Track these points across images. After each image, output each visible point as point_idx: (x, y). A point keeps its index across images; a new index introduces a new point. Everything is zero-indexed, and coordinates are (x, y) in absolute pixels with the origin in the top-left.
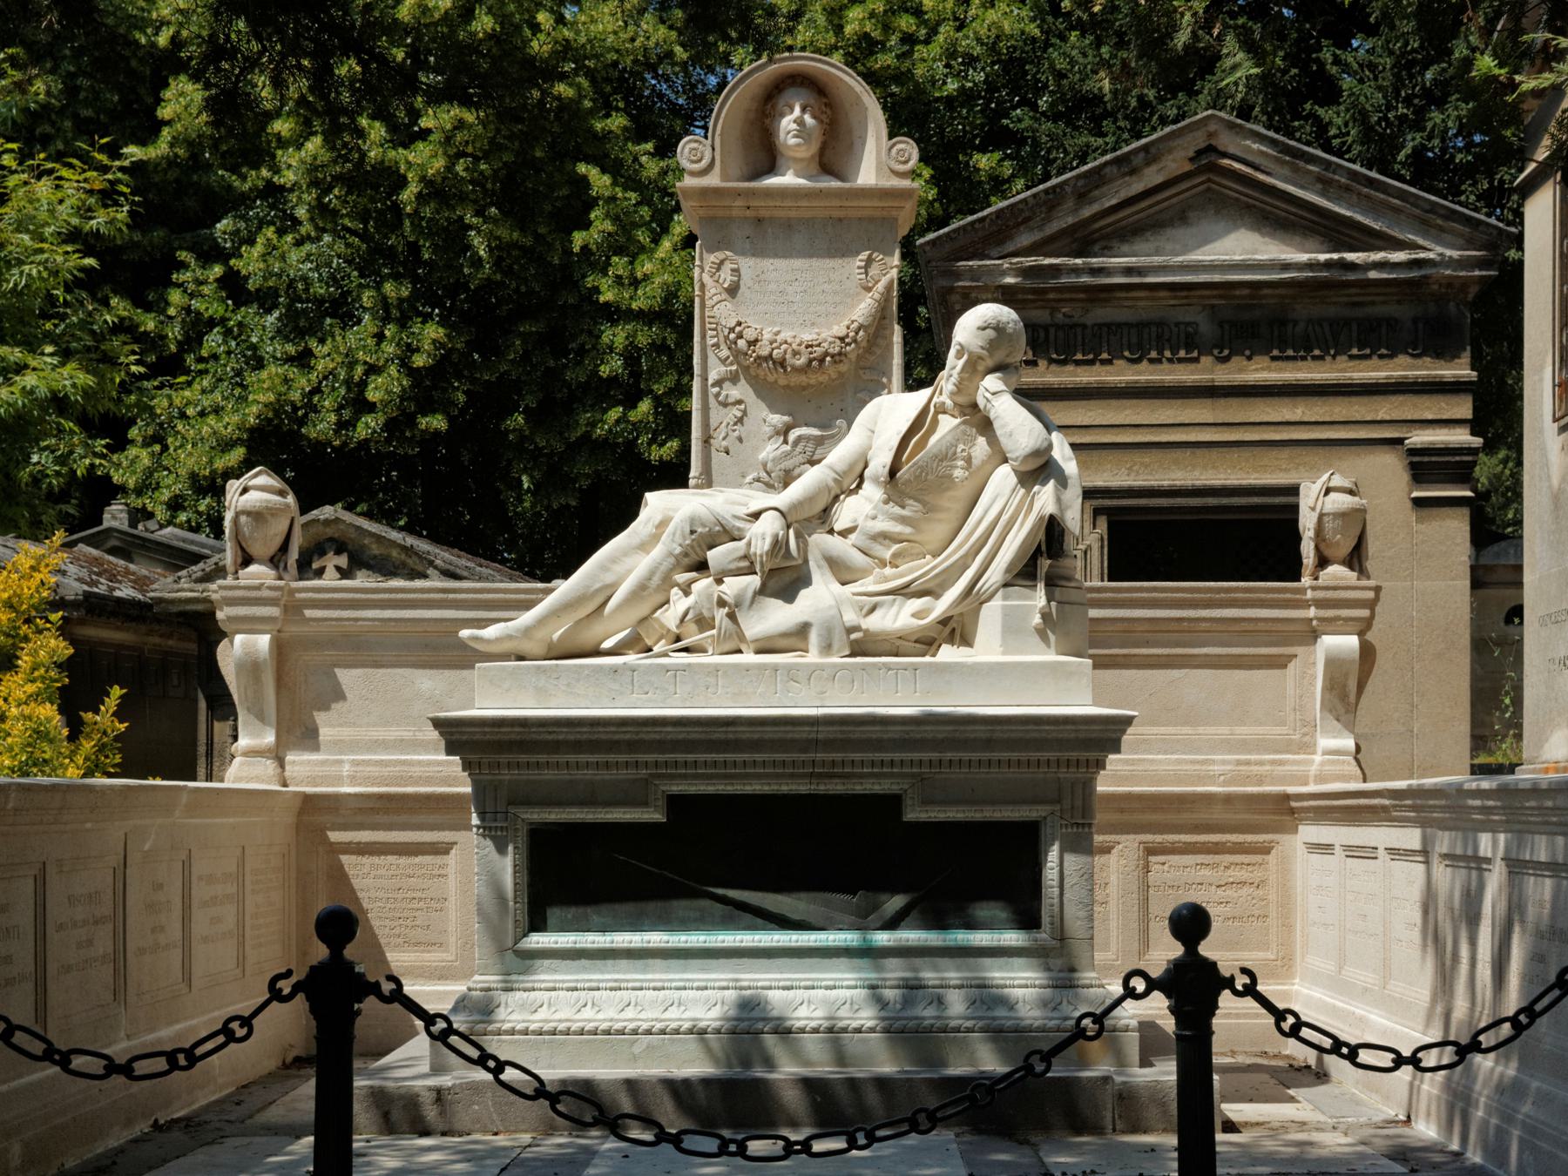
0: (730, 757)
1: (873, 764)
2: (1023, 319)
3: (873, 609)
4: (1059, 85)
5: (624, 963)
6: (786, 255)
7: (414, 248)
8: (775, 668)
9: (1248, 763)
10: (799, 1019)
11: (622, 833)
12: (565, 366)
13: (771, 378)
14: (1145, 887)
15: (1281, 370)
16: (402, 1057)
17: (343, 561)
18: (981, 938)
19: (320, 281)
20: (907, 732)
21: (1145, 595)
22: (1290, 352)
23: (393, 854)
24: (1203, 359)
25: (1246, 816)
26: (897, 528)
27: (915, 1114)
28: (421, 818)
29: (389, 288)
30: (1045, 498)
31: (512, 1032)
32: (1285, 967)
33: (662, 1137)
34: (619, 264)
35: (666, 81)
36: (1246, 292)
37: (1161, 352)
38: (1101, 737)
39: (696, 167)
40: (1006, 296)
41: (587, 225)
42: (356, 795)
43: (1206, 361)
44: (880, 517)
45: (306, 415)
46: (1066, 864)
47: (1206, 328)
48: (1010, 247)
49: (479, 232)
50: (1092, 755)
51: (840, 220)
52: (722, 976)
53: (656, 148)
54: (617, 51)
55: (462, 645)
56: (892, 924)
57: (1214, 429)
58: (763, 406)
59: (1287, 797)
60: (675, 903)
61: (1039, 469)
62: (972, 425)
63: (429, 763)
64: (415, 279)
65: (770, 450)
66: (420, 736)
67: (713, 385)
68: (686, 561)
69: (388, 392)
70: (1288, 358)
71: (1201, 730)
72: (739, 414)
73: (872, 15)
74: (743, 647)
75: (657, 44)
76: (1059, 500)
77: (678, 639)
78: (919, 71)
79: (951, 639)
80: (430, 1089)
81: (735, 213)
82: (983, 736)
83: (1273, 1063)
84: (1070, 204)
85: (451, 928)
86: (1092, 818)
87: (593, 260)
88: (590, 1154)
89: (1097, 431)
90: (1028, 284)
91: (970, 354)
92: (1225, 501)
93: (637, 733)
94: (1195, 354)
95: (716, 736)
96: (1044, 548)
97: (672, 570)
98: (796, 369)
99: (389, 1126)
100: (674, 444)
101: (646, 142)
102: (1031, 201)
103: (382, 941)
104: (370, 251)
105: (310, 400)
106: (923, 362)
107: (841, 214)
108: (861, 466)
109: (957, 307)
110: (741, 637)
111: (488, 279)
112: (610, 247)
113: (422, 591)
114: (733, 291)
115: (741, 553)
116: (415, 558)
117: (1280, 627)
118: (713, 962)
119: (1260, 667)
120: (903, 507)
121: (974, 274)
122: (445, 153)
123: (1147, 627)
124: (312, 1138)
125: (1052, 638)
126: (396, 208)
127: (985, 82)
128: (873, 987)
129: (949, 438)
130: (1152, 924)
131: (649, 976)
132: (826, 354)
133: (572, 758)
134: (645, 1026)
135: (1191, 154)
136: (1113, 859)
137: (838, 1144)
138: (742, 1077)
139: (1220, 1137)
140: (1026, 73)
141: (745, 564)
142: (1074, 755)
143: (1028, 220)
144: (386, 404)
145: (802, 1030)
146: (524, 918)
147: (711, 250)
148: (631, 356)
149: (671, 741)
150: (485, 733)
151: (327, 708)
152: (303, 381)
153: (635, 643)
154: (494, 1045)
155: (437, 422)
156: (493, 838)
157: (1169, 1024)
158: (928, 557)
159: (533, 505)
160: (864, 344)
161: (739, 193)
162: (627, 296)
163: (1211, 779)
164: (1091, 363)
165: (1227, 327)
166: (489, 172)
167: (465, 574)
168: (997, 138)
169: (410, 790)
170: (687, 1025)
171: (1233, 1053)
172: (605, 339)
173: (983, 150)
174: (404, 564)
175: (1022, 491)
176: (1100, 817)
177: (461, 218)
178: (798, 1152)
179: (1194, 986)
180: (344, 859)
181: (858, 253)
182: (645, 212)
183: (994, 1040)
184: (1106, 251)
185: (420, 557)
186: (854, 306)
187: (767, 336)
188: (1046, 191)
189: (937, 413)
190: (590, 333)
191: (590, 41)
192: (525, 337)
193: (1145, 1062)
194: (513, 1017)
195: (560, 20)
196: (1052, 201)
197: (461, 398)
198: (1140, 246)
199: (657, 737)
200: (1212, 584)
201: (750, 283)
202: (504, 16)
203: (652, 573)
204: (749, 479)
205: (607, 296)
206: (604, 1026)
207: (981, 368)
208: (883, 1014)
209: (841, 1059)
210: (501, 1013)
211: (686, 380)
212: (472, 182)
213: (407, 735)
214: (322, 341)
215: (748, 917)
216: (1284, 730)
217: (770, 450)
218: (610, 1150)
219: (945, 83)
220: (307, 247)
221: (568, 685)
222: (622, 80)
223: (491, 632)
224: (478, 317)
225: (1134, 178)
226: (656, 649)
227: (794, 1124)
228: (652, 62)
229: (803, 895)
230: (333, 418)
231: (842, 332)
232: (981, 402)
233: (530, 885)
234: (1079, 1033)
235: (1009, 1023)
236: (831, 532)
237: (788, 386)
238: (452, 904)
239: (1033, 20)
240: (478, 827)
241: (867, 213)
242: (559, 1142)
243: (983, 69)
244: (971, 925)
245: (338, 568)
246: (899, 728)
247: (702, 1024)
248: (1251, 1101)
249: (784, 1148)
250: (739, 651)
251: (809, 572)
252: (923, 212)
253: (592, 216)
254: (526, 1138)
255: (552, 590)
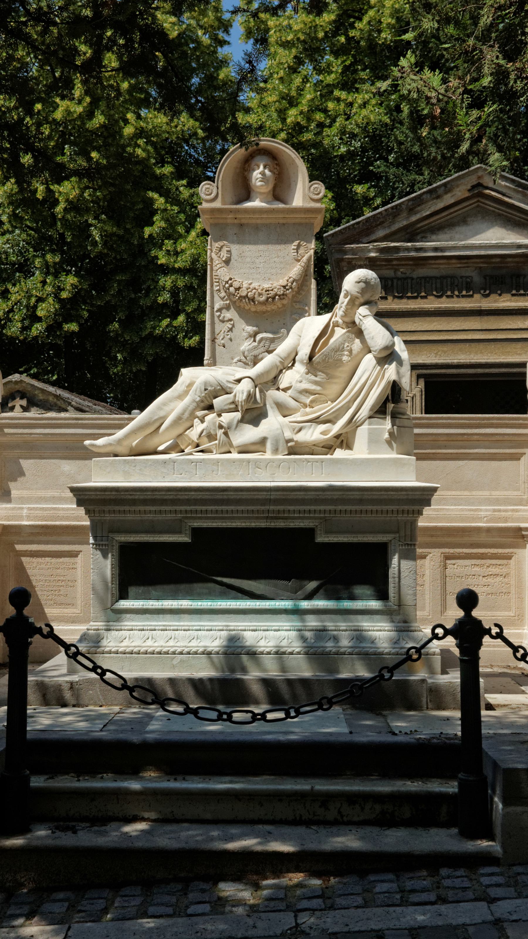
0: (224, 508)
1: (300, 512)
2: (378, 275)
3: (300, 430)
4: (400, 149)
5: (168, 616)
6: (255, 243)
7: (62, 236)
8: (249, 461)
9: (499, 511)
10: (260, 647)
11: (173, 548)
12: (140, 297)
13: (247, 308)
14: (444, 577)
15: (517, 301)
16: (52, 664)
17: (24, 402)
18: (359, 605)
19: (13, 254)
20: (318, 495)
21: (444, 421)
22: (522, 292)
23: (48, 556)
24: (475, 295)
25: (499, 539)
26: (313, 387)
27: (321, 699)
28: (64, 538)
29: (49, 257)
30: (391, 371)
31: (110, 652)
32: (519, 620)
33: (188, 710)
34: (168, 244)
35: (193, 148)
36: (498, 260)
37: (453, 292)
38: (421, 498)
39: (208, 197)
40: (371, 264)
41: (152, 224)
42: (30, 526)
43: (477, 296)
44: (304, 381)
45: (5, 323)
46: (402, 565)
47: (477, 279)
48: (373, 237)
49: (96, 228)
50: (416, 508)
51: (284, 224)
52: (220, 624)
53: (188, 183)
54: (168, 133)
55: (85, 448)
56: (310, 597)
57: (481, 332)
58: (243, 321)
59: (520, 529)
60: (196, 585)
61: (388, 356)
62: (353, 333)
63: (68, 509)
64: (62, 252)
65: (246, 345)
66: (63, 495)
67: (217, 311)
68: (202, 405)
69: (48, 311)
70: (521, 295)
71: (474, 493)
72: (230, 326)
73: (301, 113)
74: (232, 450)
75: (189, 129)
76: (398, 373)
77: (198, 446)
78: (326, 142)
79: (341, 446)
80: (67, 682)
81: (229, 221)
82: (358, 497)
83: (513, 672)
84: (404, 214)
85: (78, 596)
86: (415, 540)
87: (155, 242)
88: (150, 717)
89: (418, 334)
90: (383, 256)
91: (352, 295)
92: (487, 371)
93: (176, 495)
94: (471, 293)
95: (218, 497)
96: (390, 398)
97: (194, 410)
98: (260, 303)
99: (46, 701)
100: (197, 338)
101: (183, 180)
102: (384, 213)
103: (43, 602)
104: (40, 238)
105: (8, 316)
106: (328, 295)
107: (284, 221)
108: (294, 354)
109: (345, 269)
110: (231, 445)
111: (101, 252)
112: (163, 235)
113: (65, 419)
114: (227, 262)
115: (231, 401)
116: (61, 401)
117: (516, 438)
118: (215, 616)
119: (505, 460)
120: (316, 376)
121: (353, 251)
122: (79, 187)
123: (445, 438)
124: (6, 708)
125: (395, 445)
126: (54, 216)
127: (361, 147)
128: (299, 630)
129: (340, 340)
130: (448, 596)
131: (182, 624)
132: (276, 295)
133: (142, 508)
134: (179, 650)
135: (469, 187)
136: (427, 562)
137: (281, 715)
138: (230, 677)
139: (484, 713)
140: (382, 142)
141: (233, 406)
142: (406, 508)
143: (383, 222)
144: (47, 317)
145: (262, 653)
146: (116, 592)
147: (216, 241)
148: (174, 292)
149: (194, 499)
150: (97, 495)
151: (15, 480)
152: (4, 306)
153: (175, 448)
154: (101, 659)
155: (73, 327)
156: (102, 551)
157: (456, 651)
158: (329, 402)
159: (123, 369)
160: (296, 289)
161: (231, 211)
162: (172, 260)
163: (480, 519)
164: (416, 298)
165: (487, 278)
166: (101, 197)
167: (87, 409)
168: (366, 177)
169: (58, 523)
170: (201, 650)
171: (492, 666)
172: (161, 283)
173: (359, 183)
174: (56, 405)
175: (379, 368)
176: (420, 539)
177: (87, 221)
178: (259, 719)
179: (470, 633)
180: (24, 559)
181: (293, 242)
182: (182, 217)
183: (363, 659)
184: (424, 239)
185: (64, 400)
186: (291, 270)
187: (245, 285)
188: (392, 208)
189: (334, 326)
190: (153, 280)
191: (154, 127)
192: (119, 282)
193: (444, 672)
194: (111, 644)
195: (139, 117)
196: (396, 212)
197: (86, 314)
198: (441, 236)
199: (186, 497)
200: (480, 415)
201: (236, 258)
202: (110, 115)
203: (184, 411)
204: (235, 360)
205: (162, 261)
206: (158, 650)
207: (357, 303)
208: (305, 645)
209: (283, 669)
210: (104, 643)
211: (203, 304)
212: (92, 201)
213: (56, 494)
214: (14, 285)
215: (234, 593)
216: (519, 493)
217: (246, 345)
218: (161, 716)
219: (339, 148)
220: (7, 236)
221: (140, 470)
222: (170, 147)
223: (101, 442)
224: (96, 273)
225: (439, 200)
226: (186, 451)
227: (257, 703)
228: (187, 138)
229: (263, 581)
230: (19, 325)
231: (285, 283)
232: (357, 321)
233: (120, 575)
234: (409, 658)
235: (372, 650)
236: (278, 389)
237: (256, 312)
238: (79, 584)
239: (386, 114)
240: (93, 544)
241: (297, 221)
242: (134, 711)
243: (360, 140)
244: (352, 598)
245: (21, 406)
246: (313, 493)
247: (209, 649)
248: (501, 693)
249: (252, 718)
250: (230, 452)
251: (267, 410)
252: (328, 215)
253: (155, 219)
254: (117, 709)
255: (133, 419)
